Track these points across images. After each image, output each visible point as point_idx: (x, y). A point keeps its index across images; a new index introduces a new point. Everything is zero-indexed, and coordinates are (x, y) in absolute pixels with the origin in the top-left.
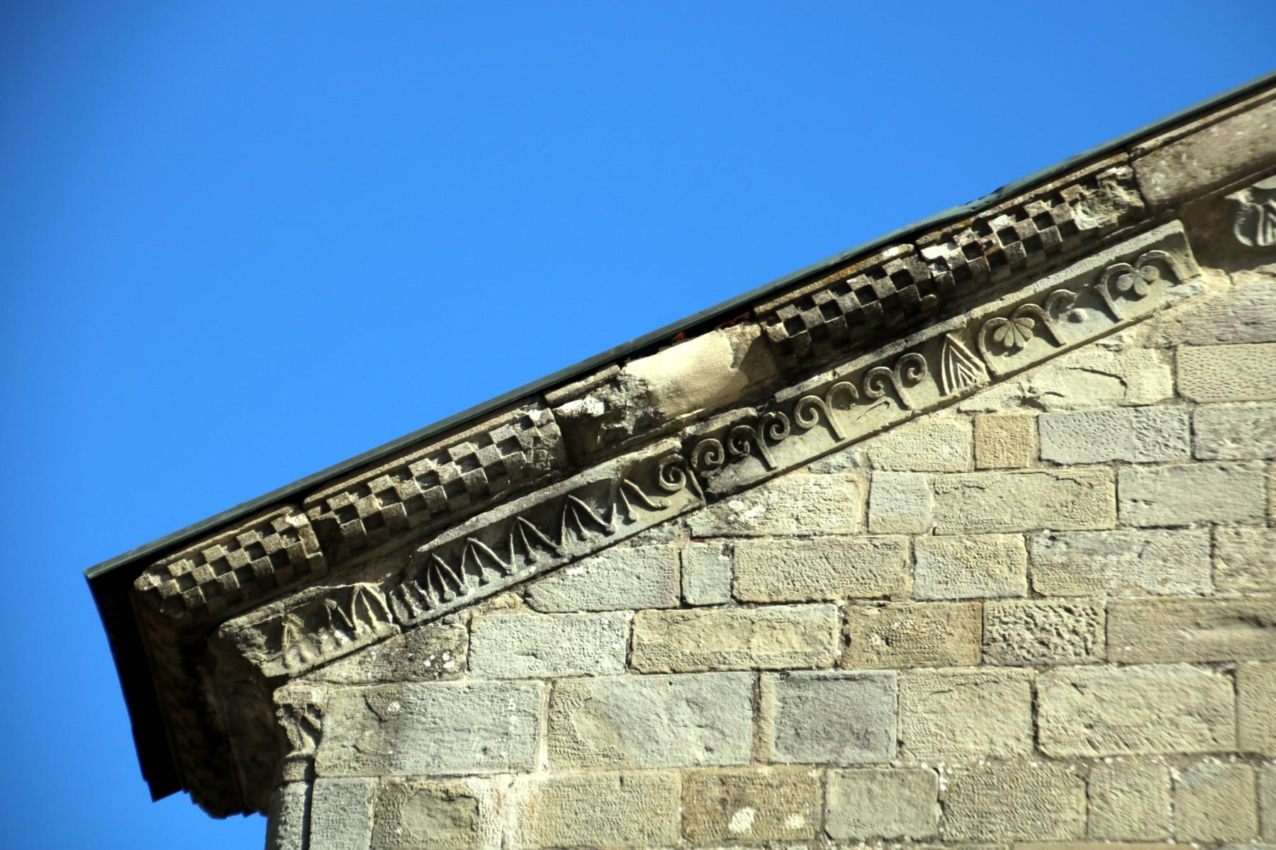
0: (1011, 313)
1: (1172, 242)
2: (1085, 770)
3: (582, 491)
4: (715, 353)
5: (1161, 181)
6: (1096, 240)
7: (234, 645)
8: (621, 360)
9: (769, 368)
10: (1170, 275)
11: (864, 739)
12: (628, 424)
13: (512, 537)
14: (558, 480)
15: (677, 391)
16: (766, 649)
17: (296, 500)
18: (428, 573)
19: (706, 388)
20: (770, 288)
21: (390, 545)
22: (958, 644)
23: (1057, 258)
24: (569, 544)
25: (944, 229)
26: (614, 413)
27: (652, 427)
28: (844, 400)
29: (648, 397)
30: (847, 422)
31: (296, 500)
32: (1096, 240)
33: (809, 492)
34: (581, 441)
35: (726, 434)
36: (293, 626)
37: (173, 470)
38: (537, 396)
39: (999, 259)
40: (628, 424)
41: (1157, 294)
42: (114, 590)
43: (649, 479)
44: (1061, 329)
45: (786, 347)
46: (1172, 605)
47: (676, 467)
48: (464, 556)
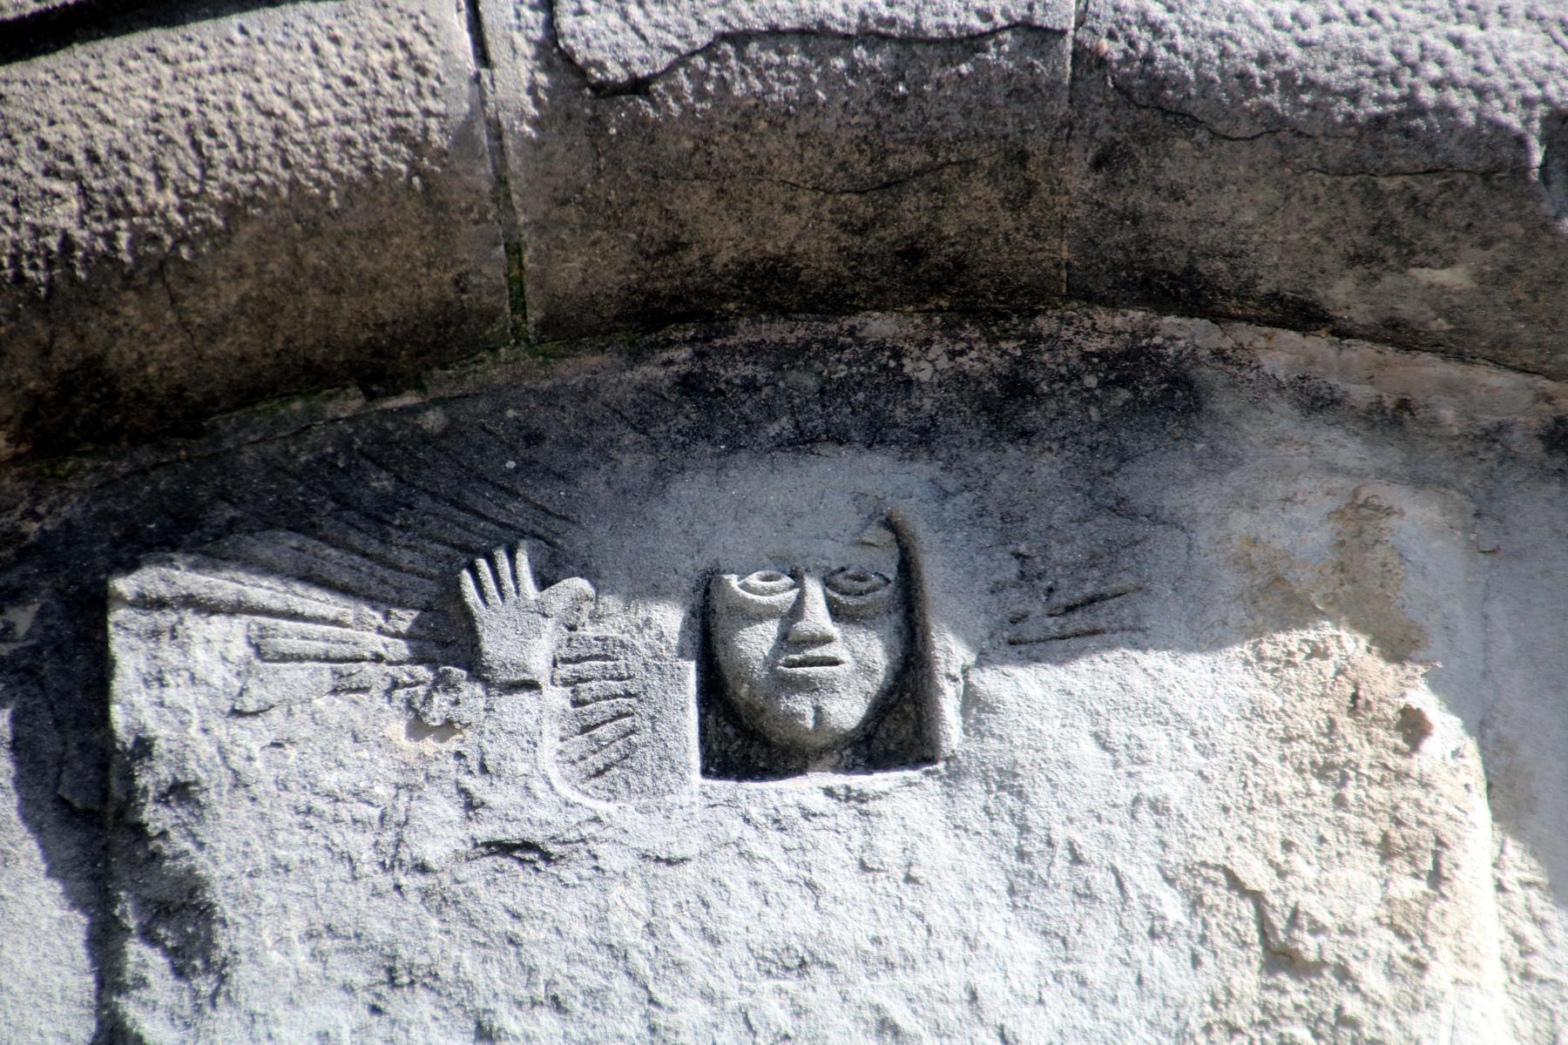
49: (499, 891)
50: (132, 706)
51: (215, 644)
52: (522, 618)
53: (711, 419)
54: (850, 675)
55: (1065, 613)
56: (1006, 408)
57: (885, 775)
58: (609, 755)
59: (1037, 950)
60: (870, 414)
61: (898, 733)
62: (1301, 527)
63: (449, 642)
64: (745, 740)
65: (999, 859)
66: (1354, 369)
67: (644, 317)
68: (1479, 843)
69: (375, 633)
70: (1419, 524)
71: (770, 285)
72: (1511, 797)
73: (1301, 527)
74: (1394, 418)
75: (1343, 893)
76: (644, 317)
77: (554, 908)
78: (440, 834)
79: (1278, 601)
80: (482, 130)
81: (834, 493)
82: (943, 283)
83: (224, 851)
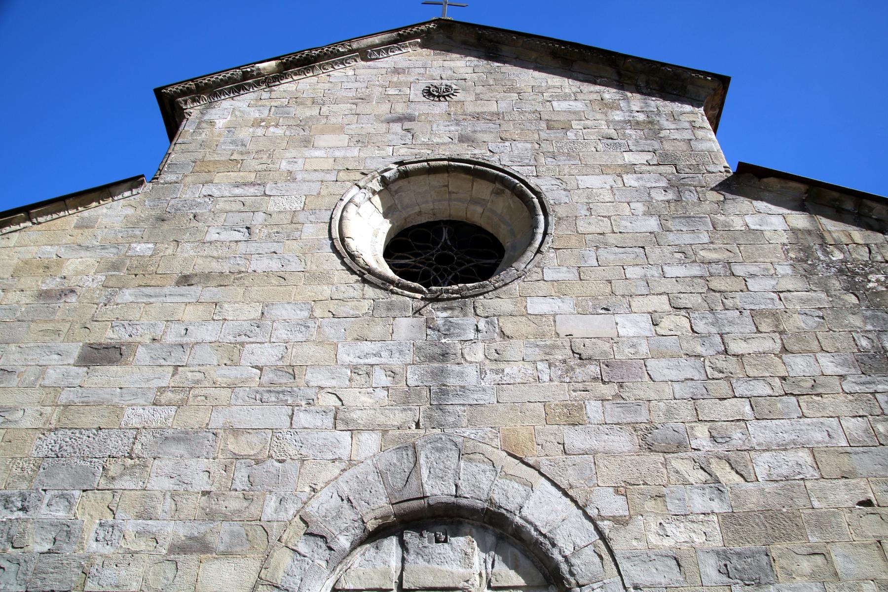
0: (327, 63)
1: (357, 56)
2: (327, 117)
3: (246, 84)
4: (273, 63)
5: (355, 46)
6: (343, 54)
7: (178, 103)
8: (255, 63)
9: (282, 67)
10: (356, 61)
11: (288, 114)
12: (255, 73)
13: (231, 90)
14: (241, 82)
15: (264, 69)
16: (273, 104)
17: (192, 80)
18: (215, 95)
19: (270, 69)
20: (445, 586)
21: (209, 90)
22: (309, 103)
23: (336, 56)
24: (242, 92)
25: (316, 49)
26: (252, 71)
27: (259, 74)
28: (296, 74)
29: (259, 69)
30: (295, 78)
31: (192, 80)
32: (343, 54)
33: (287, 86)
34: (246, 76)
35: (273, 77)
36: (189, 101)
37: (172, 76)
38: (238, 68)
39: (325, 54)
40: (255, 73)
41: (353, 63)
42: (158, 92)
43: (258, 84)
44: (336, 67)
45: (285, 64)
46: (348, 97)
47: (263, 82)
48: (222, 93)
49: (424, 549)
50: (405, 538)
51: (409, 535)
52: (426, 534)
53: (436, 524)
54: (443, 537)
55: (455, 535)
56: (452, 523)
57: (536, 74)
58: (430, 542)
59: (358, 556)
60: (445, 524)
61: (445, 541)
62: (468, 530)
63: (421, 535)
64: (437, 541)
65: (877, 317)
66: (470, 521)
67: (432, 517)
68: (476, 548)
69: (418, 535)
70: (474, 530)
71: (439, 516)
72: (478, 546)
73: (468, 530)
74: (472, 524)
75: (469, 551)
76: (432, 517)
77: (427, 551)
78: (421, 546)
79: (466, 534)
80: (424, 507)
81: (443, 527)
82: (449, 516)
83: (409, 546)
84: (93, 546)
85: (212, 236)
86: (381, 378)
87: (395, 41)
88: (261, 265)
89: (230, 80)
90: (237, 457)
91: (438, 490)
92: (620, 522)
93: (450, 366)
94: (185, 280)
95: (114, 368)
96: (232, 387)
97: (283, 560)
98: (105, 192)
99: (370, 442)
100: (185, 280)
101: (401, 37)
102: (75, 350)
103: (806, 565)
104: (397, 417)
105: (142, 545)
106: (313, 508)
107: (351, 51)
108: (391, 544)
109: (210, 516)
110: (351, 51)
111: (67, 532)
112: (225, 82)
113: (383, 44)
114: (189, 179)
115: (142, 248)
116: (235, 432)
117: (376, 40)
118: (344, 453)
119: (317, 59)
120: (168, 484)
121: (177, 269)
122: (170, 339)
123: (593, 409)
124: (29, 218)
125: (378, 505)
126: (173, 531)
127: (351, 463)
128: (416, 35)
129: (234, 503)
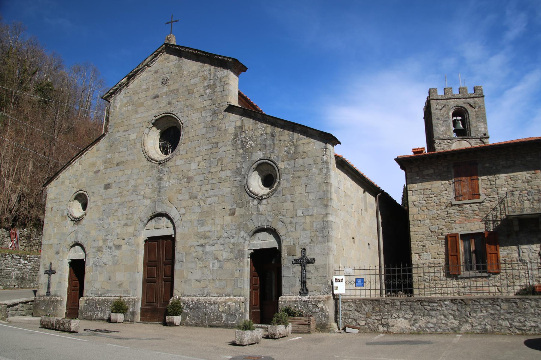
5: (144, 64)
14: (119, 89)
84: (113, 226)
85: (121, 150)
86: (150, 186)
87: (155, 57)
88: (131, 157)
89: (117, 89)
90: (130, 207)
91: (159, 210)
92: (184, 215)
93: (162, 182)
94: (118, 165)
95: (110, 190)
96: (128, 191)
97: (137, 225)
98: (98, 139)
99: (149, 201)
100: (118, 165)
101: (156, 55)
102: (103, 186)
103: (210, 222)
104: (153, 195)
105: (119, 225)
106: (141, 216)
107: (144, 66)
108: (153, 220)
109: (127, 219)
110: (144, 66)
111: (109, 224)
112: (116, 90)
113: (152, 60)
114: (114, 131)
115: (109, 156)
116: (129, 202)
117: (149, 59)
118: (145, 204)
119: (136, 72)
120: (121, 214)
121: (116, 161)
122: (117, 181)
123: (184, 190)
124: (87, 150)
125: (151, 214)
126: (123, 222)
127: (146, 206)
128: (160, 52)
129: (130, 216)
